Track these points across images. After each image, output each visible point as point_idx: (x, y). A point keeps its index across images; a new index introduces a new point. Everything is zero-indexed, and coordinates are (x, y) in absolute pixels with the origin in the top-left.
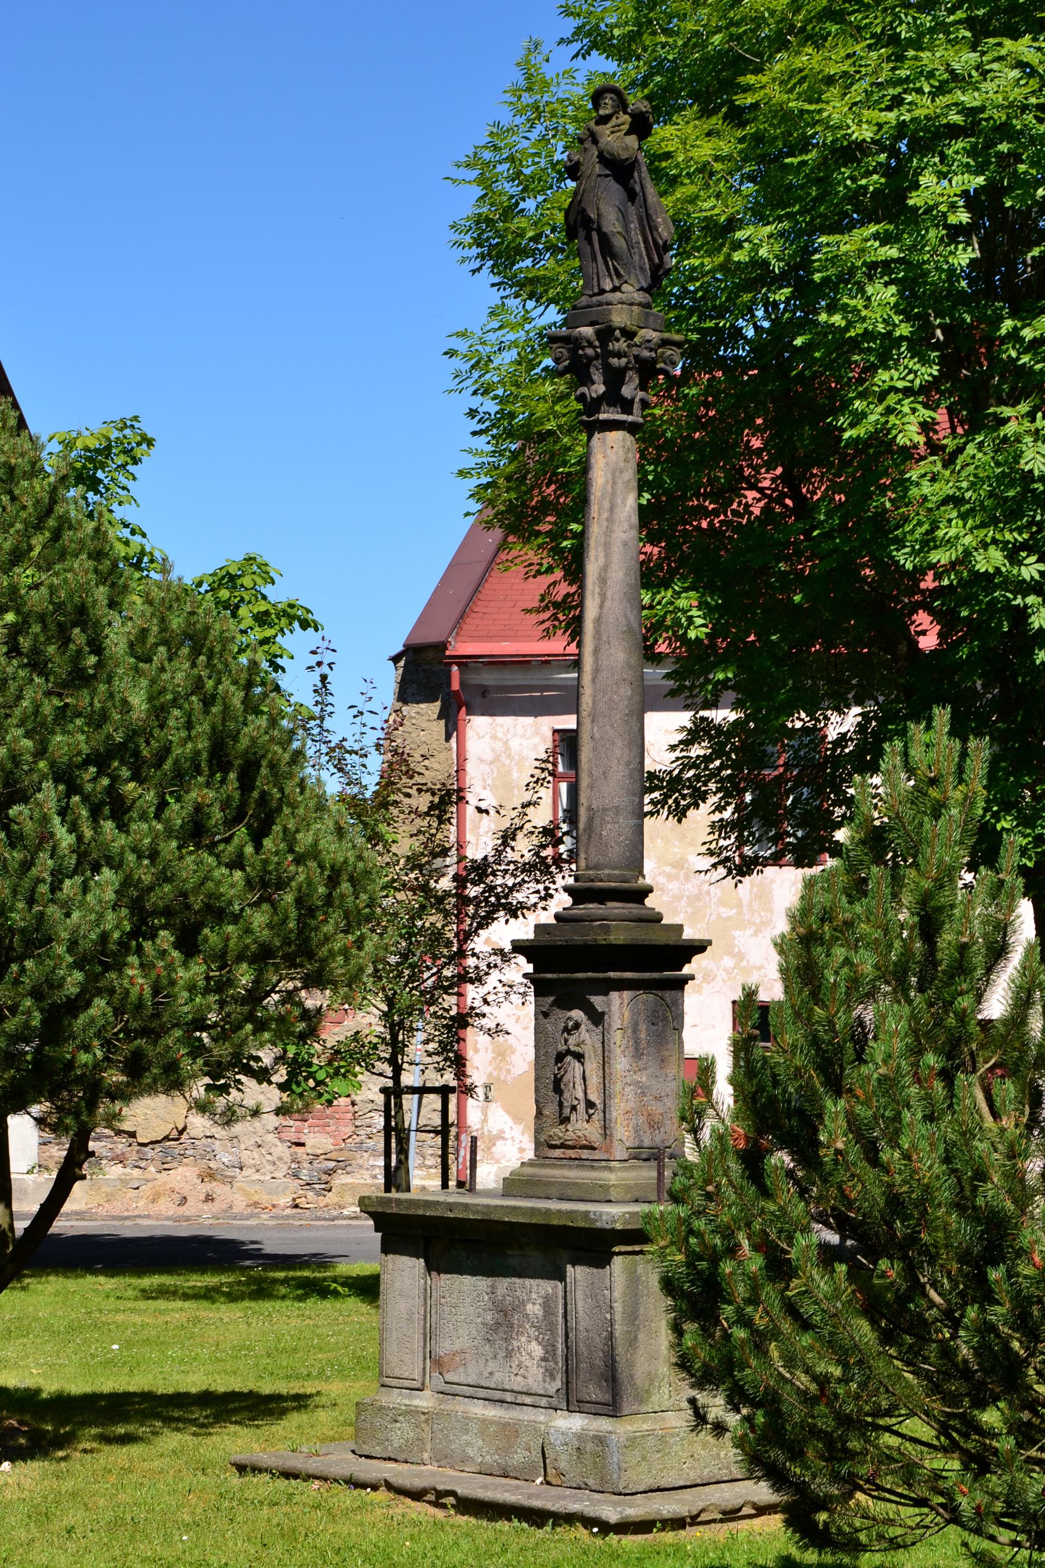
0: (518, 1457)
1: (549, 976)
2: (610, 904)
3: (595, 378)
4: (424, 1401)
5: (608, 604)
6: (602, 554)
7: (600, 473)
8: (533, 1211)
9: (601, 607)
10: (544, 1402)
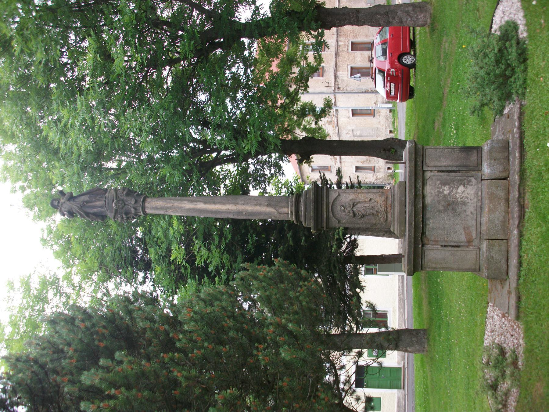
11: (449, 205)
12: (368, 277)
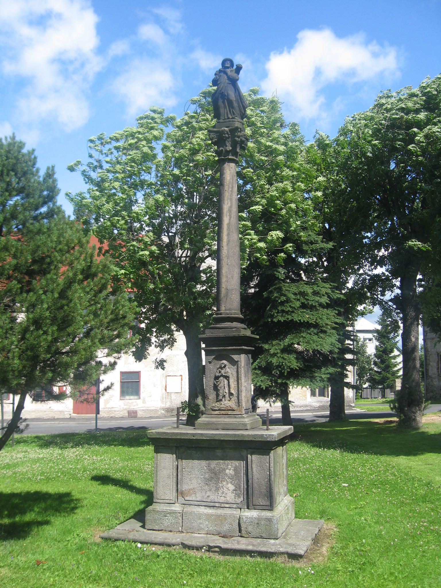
0: (226, 528)
1: (246, 348)
2: (234, 323)
3: (227, 145)
4: (177, 508)
5: (232, 219)
6: (230, 202)
7: (228, 176)
8: (194, 435)
9: (230, 220)
10: (235, 506)
11: (216, 474)
12: (29, 397)
